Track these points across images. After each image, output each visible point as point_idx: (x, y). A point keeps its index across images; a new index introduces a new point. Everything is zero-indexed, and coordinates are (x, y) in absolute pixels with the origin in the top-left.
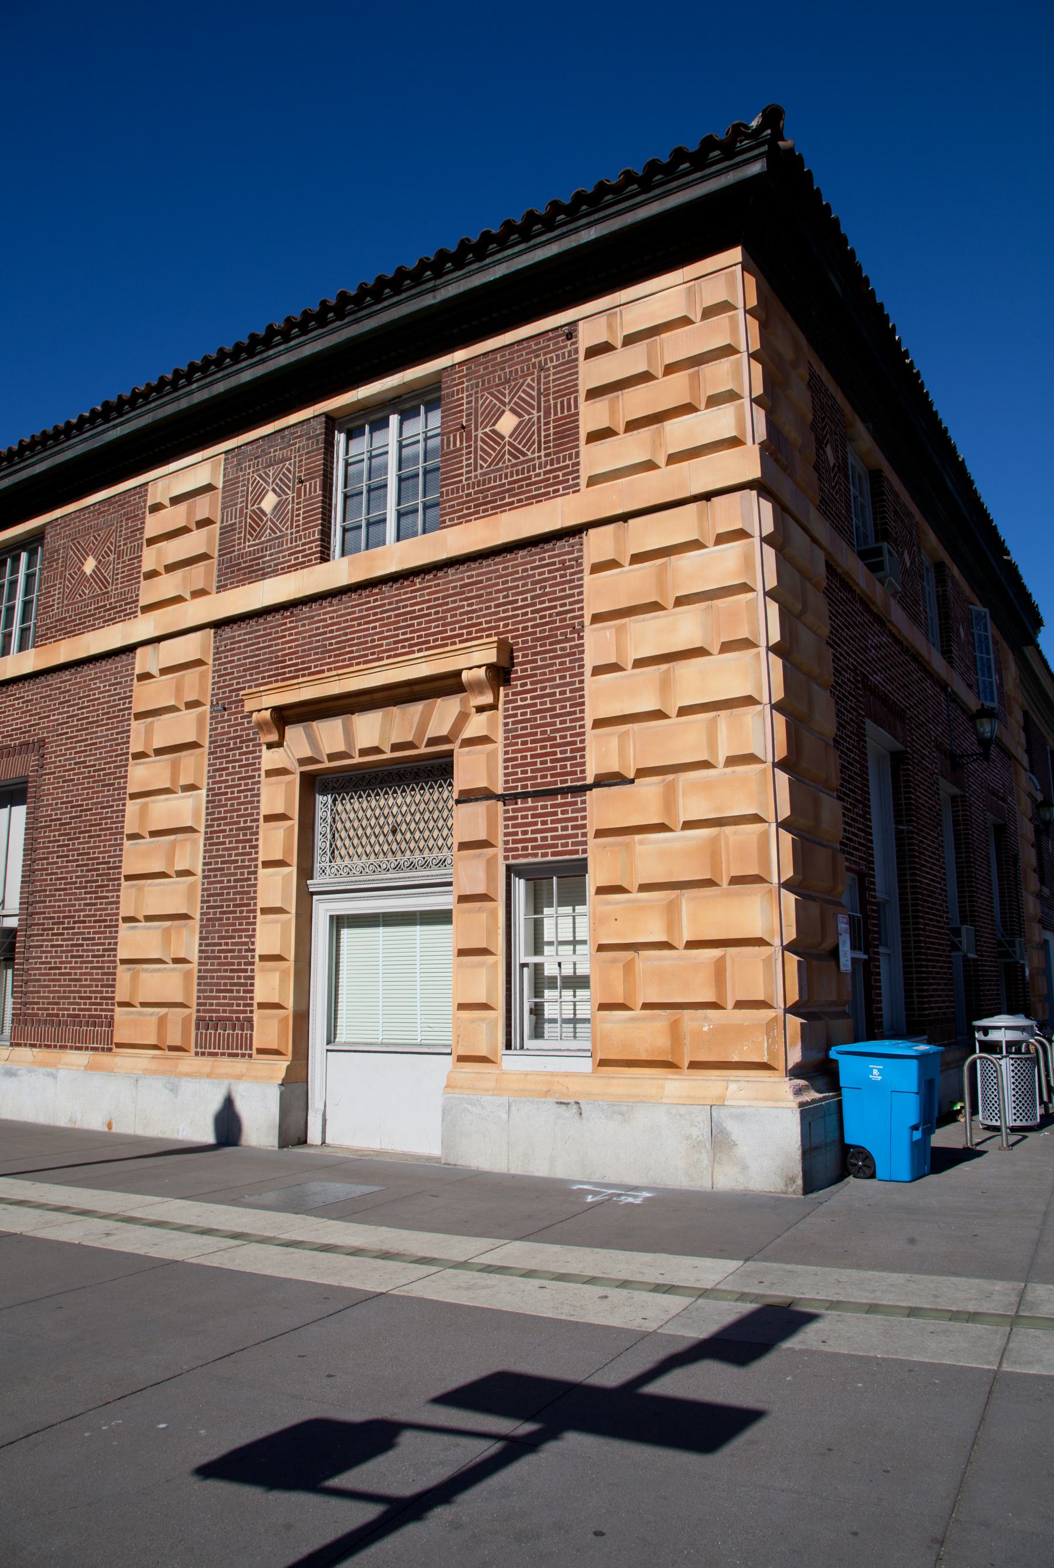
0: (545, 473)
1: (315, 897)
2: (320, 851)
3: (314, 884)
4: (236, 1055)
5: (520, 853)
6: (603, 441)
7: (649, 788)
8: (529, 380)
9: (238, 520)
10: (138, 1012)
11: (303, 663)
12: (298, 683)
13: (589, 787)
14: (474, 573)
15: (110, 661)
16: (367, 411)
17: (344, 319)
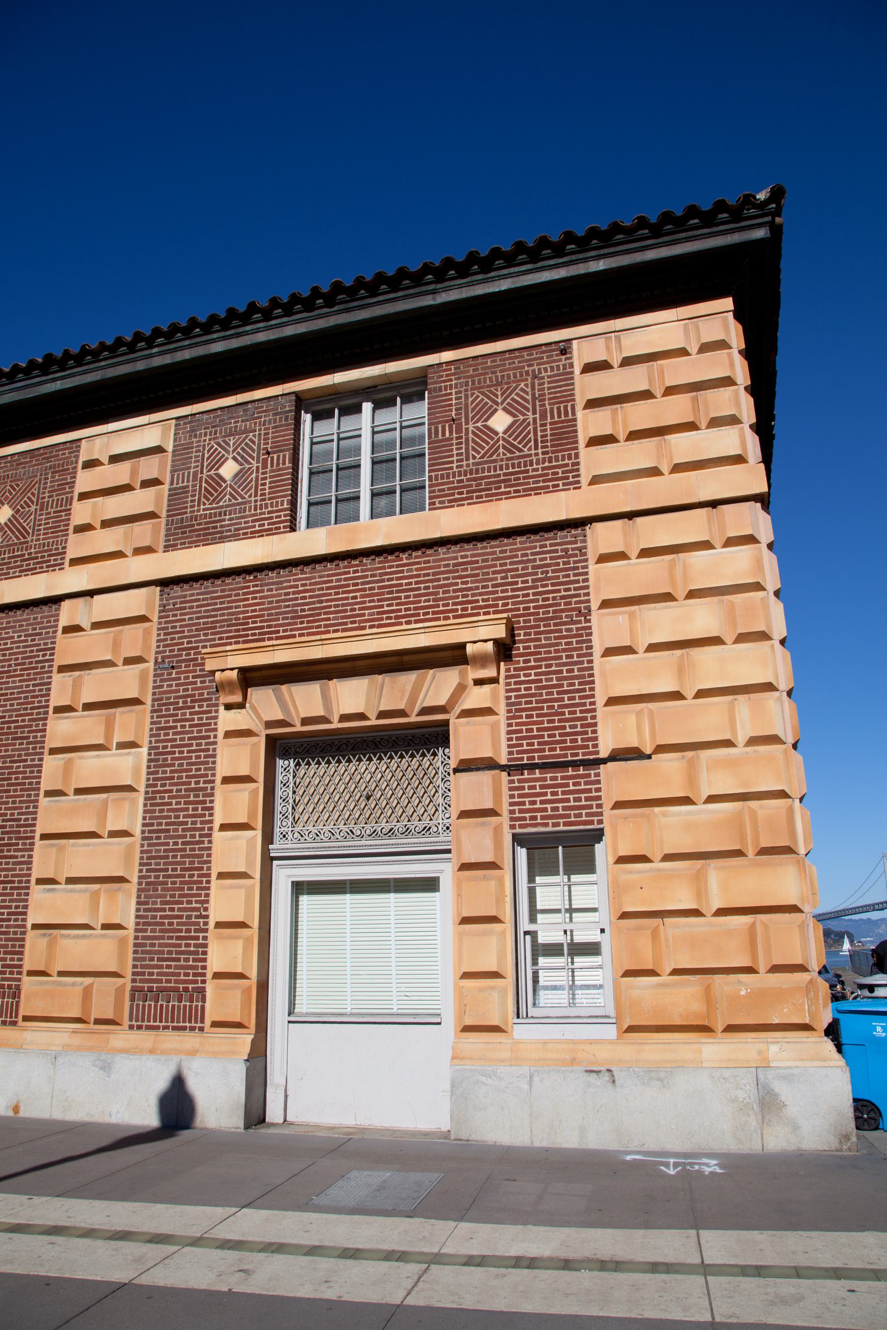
0: (543, 469)
1: (275, 863)
2: (280, 816)
3: (277, 847)
4: (184, 1028)
5: (528, 822)
6: (604, 446)
7: (669, 762)
8: (522, 385)
9: (191, 483)
10: (54, 982)
11: (269, 626)
12: (273, 646)
13: (604, 761)
14: (468, 553)
15: (27, 611)
16: (337, 396)
17: (333, 307)
